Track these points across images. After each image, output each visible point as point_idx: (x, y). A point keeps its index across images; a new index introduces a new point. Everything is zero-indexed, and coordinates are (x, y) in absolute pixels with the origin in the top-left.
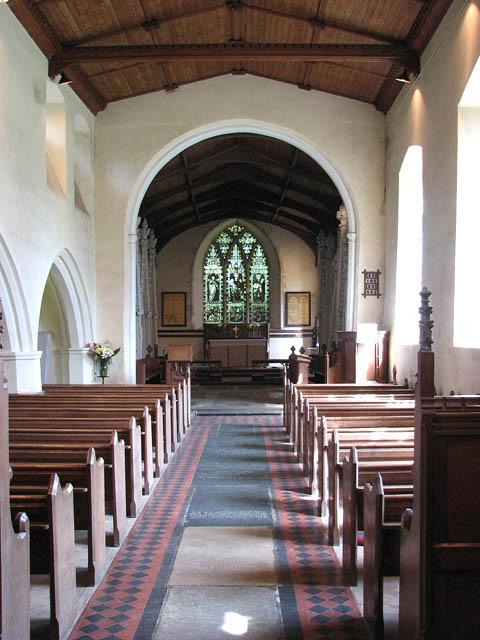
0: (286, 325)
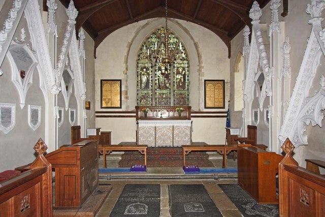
0: (224, 108)
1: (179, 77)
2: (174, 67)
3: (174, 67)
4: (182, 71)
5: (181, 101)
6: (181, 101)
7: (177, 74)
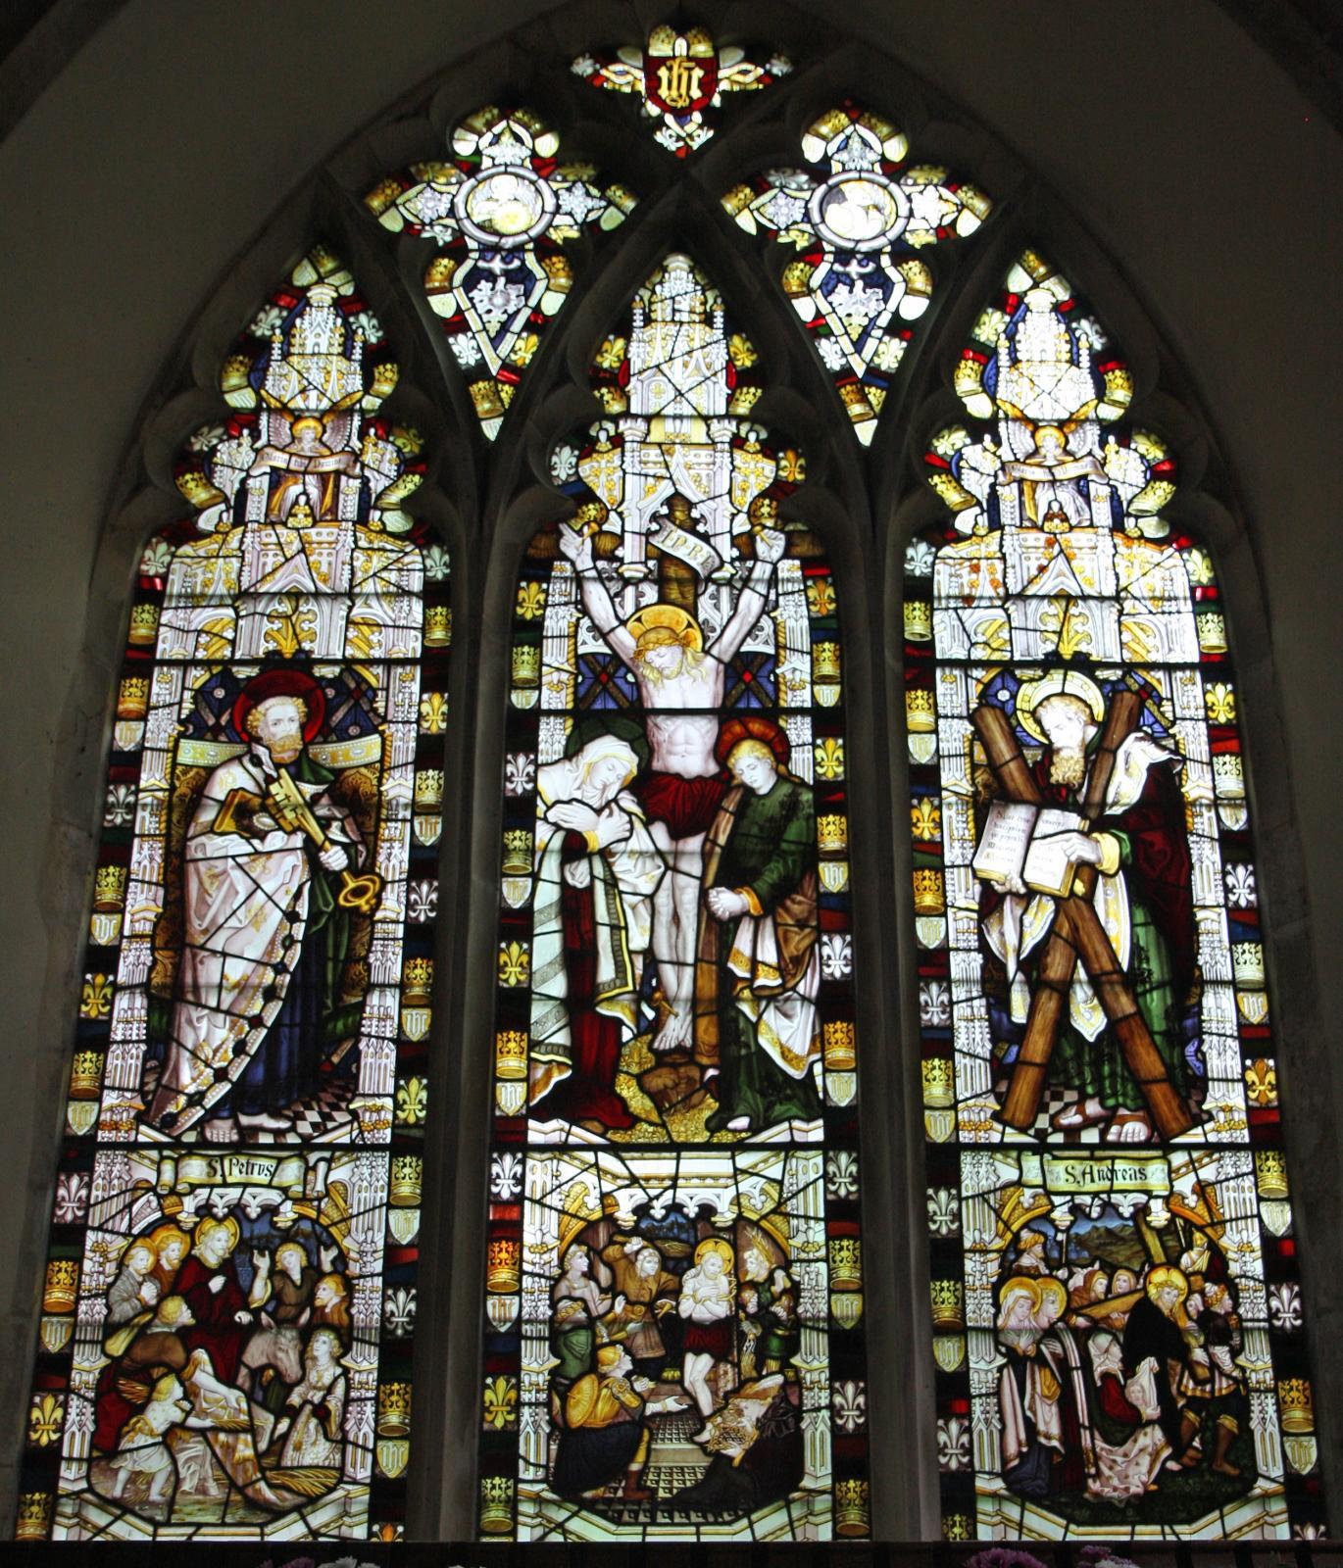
1: (1049, 869)
2: (142, 661)
3: (142, 661)
4: (1100, 753)
5: (1120, 1422)
6: (1120, 1422)
7: (984, 806)
